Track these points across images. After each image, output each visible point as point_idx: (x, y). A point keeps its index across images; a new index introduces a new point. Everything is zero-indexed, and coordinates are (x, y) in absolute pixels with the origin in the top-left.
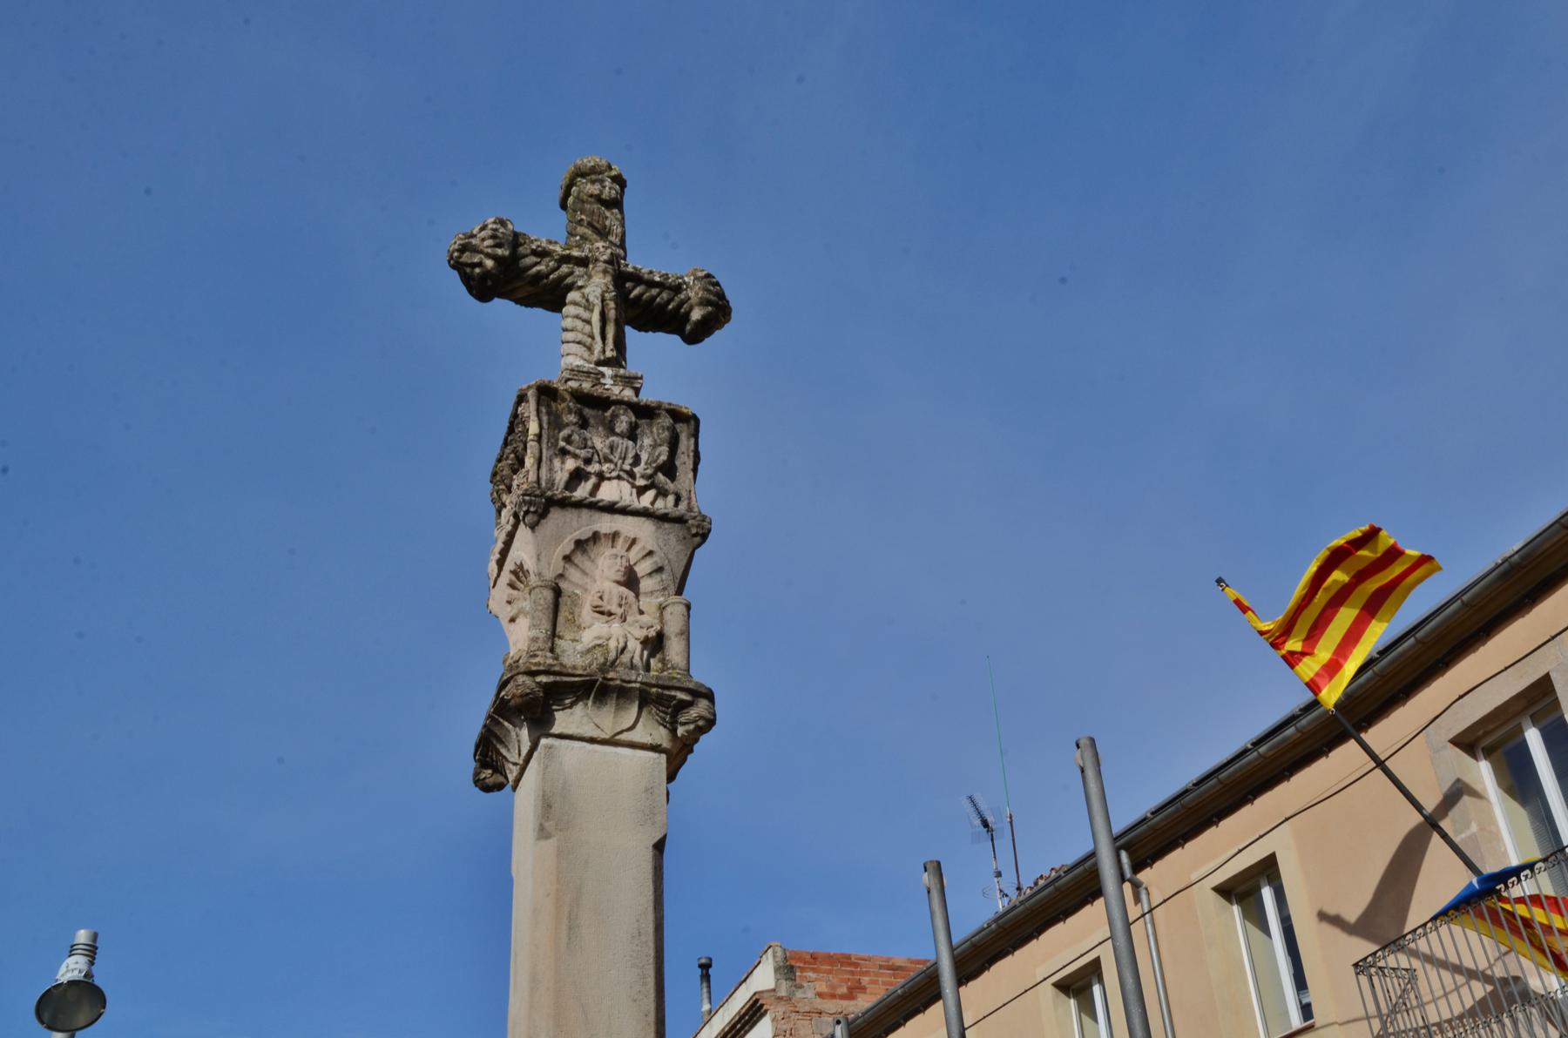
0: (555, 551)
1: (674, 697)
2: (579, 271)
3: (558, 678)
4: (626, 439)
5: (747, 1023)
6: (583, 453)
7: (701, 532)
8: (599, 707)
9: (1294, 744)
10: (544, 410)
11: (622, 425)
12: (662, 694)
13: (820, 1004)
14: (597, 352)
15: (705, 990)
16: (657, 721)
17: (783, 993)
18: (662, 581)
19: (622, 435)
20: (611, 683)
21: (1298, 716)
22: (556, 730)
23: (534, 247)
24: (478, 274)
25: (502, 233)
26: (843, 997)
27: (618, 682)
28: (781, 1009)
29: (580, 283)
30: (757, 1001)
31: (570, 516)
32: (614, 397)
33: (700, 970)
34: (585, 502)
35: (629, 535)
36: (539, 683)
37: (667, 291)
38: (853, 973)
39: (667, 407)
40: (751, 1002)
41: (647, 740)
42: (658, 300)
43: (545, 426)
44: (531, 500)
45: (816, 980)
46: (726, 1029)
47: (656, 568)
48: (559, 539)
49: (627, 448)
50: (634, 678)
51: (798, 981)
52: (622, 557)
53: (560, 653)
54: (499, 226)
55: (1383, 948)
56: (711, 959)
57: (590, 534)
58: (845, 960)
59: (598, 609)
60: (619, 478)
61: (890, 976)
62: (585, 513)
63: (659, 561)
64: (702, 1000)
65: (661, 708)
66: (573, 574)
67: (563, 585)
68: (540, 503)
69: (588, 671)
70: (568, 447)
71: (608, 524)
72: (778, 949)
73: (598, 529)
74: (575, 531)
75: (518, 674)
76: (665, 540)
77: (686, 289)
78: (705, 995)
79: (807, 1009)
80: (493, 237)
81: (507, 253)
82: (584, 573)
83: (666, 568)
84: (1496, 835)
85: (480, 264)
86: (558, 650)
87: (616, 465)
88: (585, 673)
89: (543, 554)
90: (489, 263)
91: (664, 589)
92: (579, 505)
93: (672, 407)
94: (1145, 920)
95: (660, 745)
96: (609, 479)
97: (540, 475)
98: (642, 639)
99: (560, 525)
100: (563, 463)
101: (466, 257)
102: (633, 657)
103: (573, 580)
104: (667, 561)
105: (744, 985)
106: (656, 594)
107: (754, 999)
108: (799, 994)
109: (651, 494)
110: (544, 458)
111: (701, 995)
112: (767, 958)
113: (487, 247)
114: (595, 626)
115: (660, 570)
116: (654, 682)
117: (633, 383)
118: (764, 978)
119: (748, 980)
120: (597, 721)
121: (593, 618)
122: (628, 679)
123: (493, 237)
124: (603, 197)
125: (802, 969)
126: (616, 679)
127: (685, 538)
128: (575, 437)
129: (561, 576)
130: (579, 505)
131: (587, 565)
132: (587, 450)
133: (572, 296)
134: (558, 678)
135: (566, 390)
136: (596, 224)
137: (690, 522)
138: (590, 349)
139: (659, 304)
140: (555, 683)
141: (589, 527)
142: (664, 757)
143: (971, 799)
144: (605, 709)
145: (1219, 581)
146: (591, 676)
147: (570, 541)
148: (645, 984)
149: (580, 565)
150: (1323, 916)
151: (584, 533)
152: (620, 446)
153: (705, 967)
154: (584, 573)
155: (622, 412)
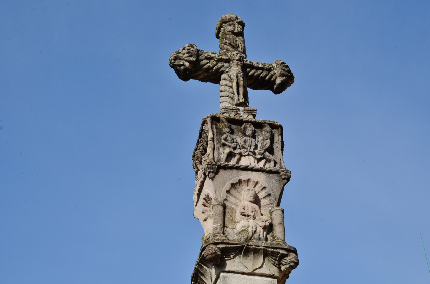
1: (279, 253)
2: (226, 65)
3: (227, 246)
6: (233, 145)
10: (214, 127)
11: (249, 132)
16: (272, 264)
18: (270, 200)
19: (249, 136)
20: (251, 247)
22: (227, 269)
23: (206, 56)
25: (192, 50)
27: (254, 246)
29: (227, 70)
31: (228, 172)
34: (234, 166)
36: (218, 248)
39: (268, 122)
41: (268, 272)
42: (261, 75)
43: (215, 134)
44: (211, 167)
48: (224, 184)
50: (260, 244)
52: (252, 190)
54: (190, 48)
59: (243, 214)
60: (249, 155)
62: (235, 171)
63: (268, 191)
65: (273, 258)
66: (231, 199)
67: (227, 204)
69: (240, 242)
70: (226, 143)
71: (245, 176)
74: (231, 180)
77: (273, 70)
80: (188, 52)
81: (194, 59)
82: (236, 198)
86: (226, 233)
87: (247, 149)
88: (239, 243)
90: (187, 64)
91: (272, 204)
92: (232, 168)
93: (270, 122)
95: (274, 275)
96: (244, 156)
99: (224, 177)
103: (231, 201)
104: (272, 191)
106: (268, 206)
109: (263, 161)
113: (186, 57)
117: (252, 113)
120: (245, 264)
121: (241, 218)
124: (235, 31)
127: (279, 181)
128: (229, 138)
129: (226, 200)
130: (232, 168)
131: (237, 194)
133: (224, 76)
134: (227, 246)
135: (224, 118)
136: (232, 44)
139: (262, 77)
141: (237, 178)
147: (229, 184)
149: (234, 194)
151: (235, 180)
154: (236, 198)
155: (248, 126)
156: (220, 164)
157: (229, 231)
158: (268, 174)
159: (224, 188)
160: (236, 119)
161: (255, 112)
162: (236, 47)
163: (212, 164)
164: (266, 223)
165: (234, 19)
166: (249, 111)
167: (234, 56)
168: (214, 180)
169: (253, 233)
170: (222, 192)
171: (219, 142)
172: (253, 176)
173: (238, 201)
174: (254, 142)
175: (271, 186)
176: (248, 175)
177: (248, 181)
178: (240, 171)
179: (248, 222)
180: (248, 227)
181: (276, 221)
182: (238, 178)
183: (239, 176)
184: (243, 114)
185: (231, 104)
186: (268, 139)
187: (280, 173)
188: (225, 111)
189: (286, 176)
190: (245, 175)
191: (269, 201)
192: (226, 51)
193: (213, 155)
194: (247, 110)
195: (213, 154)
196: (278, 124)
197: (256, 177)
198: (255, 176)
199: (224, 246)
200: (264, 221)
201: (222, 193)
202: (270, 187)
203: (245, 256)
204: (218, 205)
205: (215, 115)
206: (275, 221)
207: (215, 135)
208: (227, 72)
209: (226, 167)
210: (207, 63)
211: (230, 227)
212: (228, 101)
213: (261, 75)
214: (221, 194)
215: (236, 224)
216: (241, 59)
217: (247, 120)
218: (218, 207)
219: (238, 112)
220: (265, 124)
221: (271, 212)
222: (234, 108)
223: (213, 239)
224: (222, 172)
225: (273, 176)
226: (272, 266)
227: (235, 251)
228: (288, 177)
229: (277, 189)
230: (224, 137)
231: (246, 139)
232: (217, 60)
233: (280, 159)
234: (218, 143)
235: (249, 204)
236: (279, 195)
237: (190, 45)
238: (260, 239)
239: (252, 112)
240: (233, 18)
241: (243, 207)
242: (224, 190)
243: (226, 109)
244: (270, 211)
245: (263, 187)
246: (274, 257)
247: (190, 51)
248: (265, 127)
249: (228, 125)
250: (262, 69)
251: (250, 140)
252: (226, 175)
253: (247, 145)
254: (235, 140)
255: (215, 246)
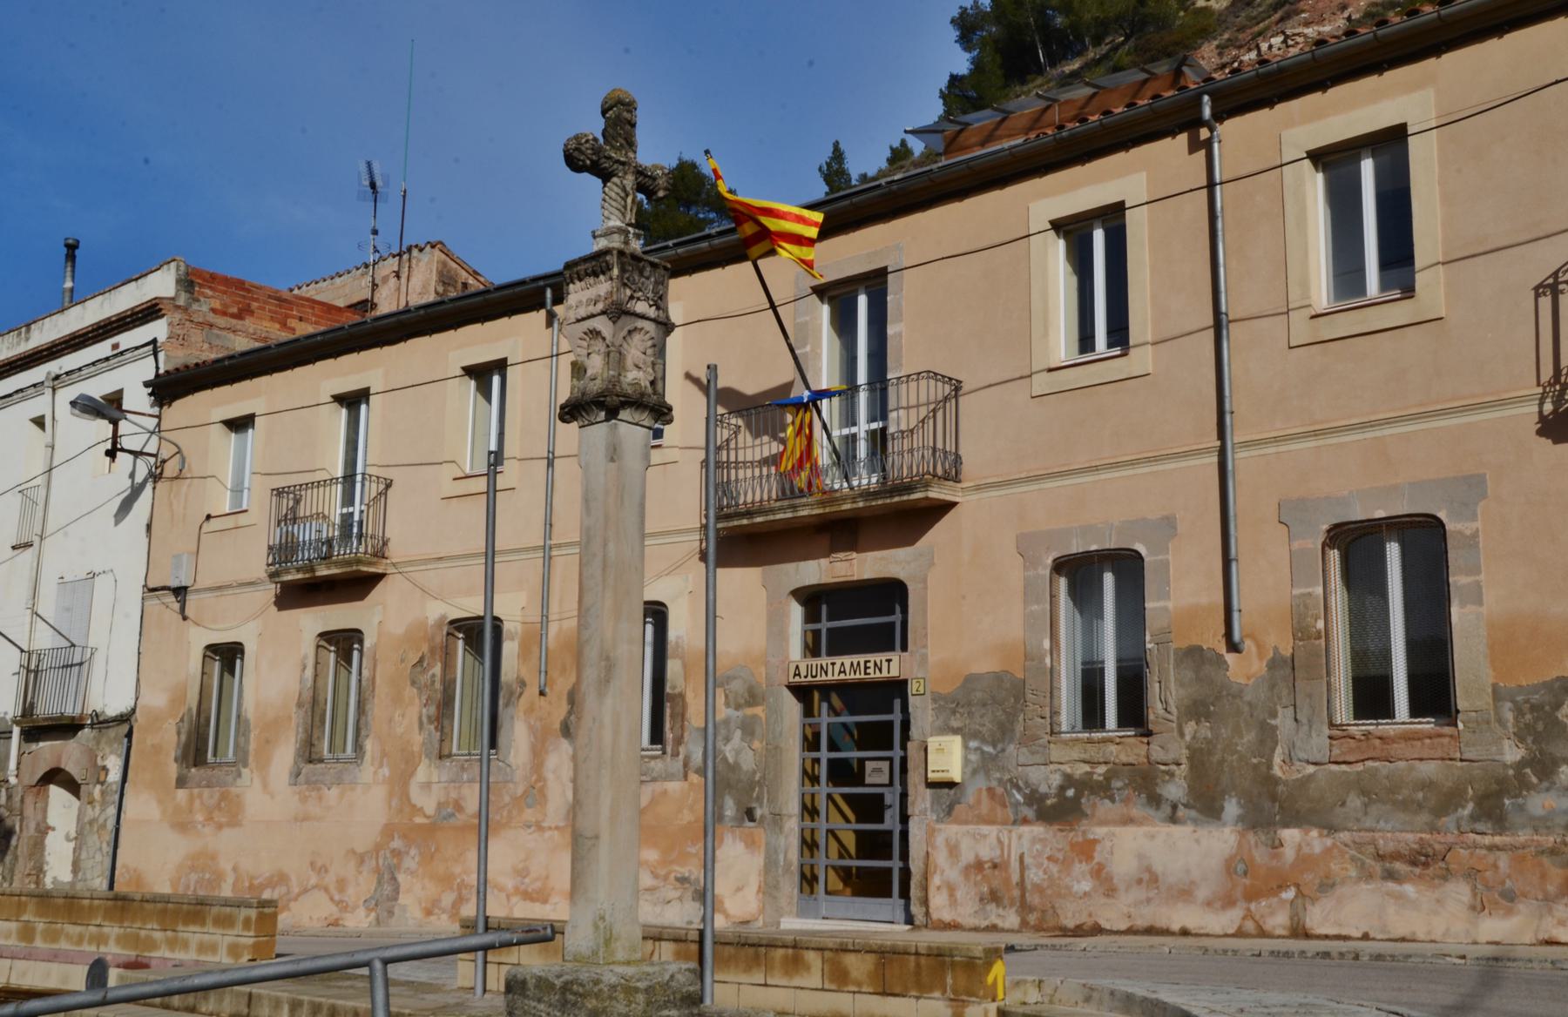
2: (621, 167)
5: (138, 319)
9: (703, 253)
13: (212, 318)
14: (628, 218)
15: (69, 269)
17: (181, 302)
21: (714, 236)
22: (619, 417)
26: (233, 316)
28: (178, 316)
30: (157, 304)
33: (65, 249)
38: (244, 297)
40: (149, 304)
45: (212, 297)
46: (114, 319)
48: (622, 329)
51: (196, 295)
55: (730, 413)
56: (78, 242)
58: (240, 285)
61: (276, 306)
64: (65, 277)
72: (182, 264)
78: (69, 274)
79: (201, 320)
84: (819, 356)
85: (583, 161)
90: (588, 162)
94: (558, 349)
101: (576, 154)
105: (134, 283)
107: (154, 302)
108: (195, 307)
111: (65, 272)
112: (169, 269)
118: (162, 284)
119: (140, 281)
123: (592, 149)
125: (201, 286)
133: (615, 179)
138: (624, 217)
143: (369, 164)
145: (707, 152)
150: (688, 376)
151: (630, 327)
153: (72, 248)
177: (642, 329)
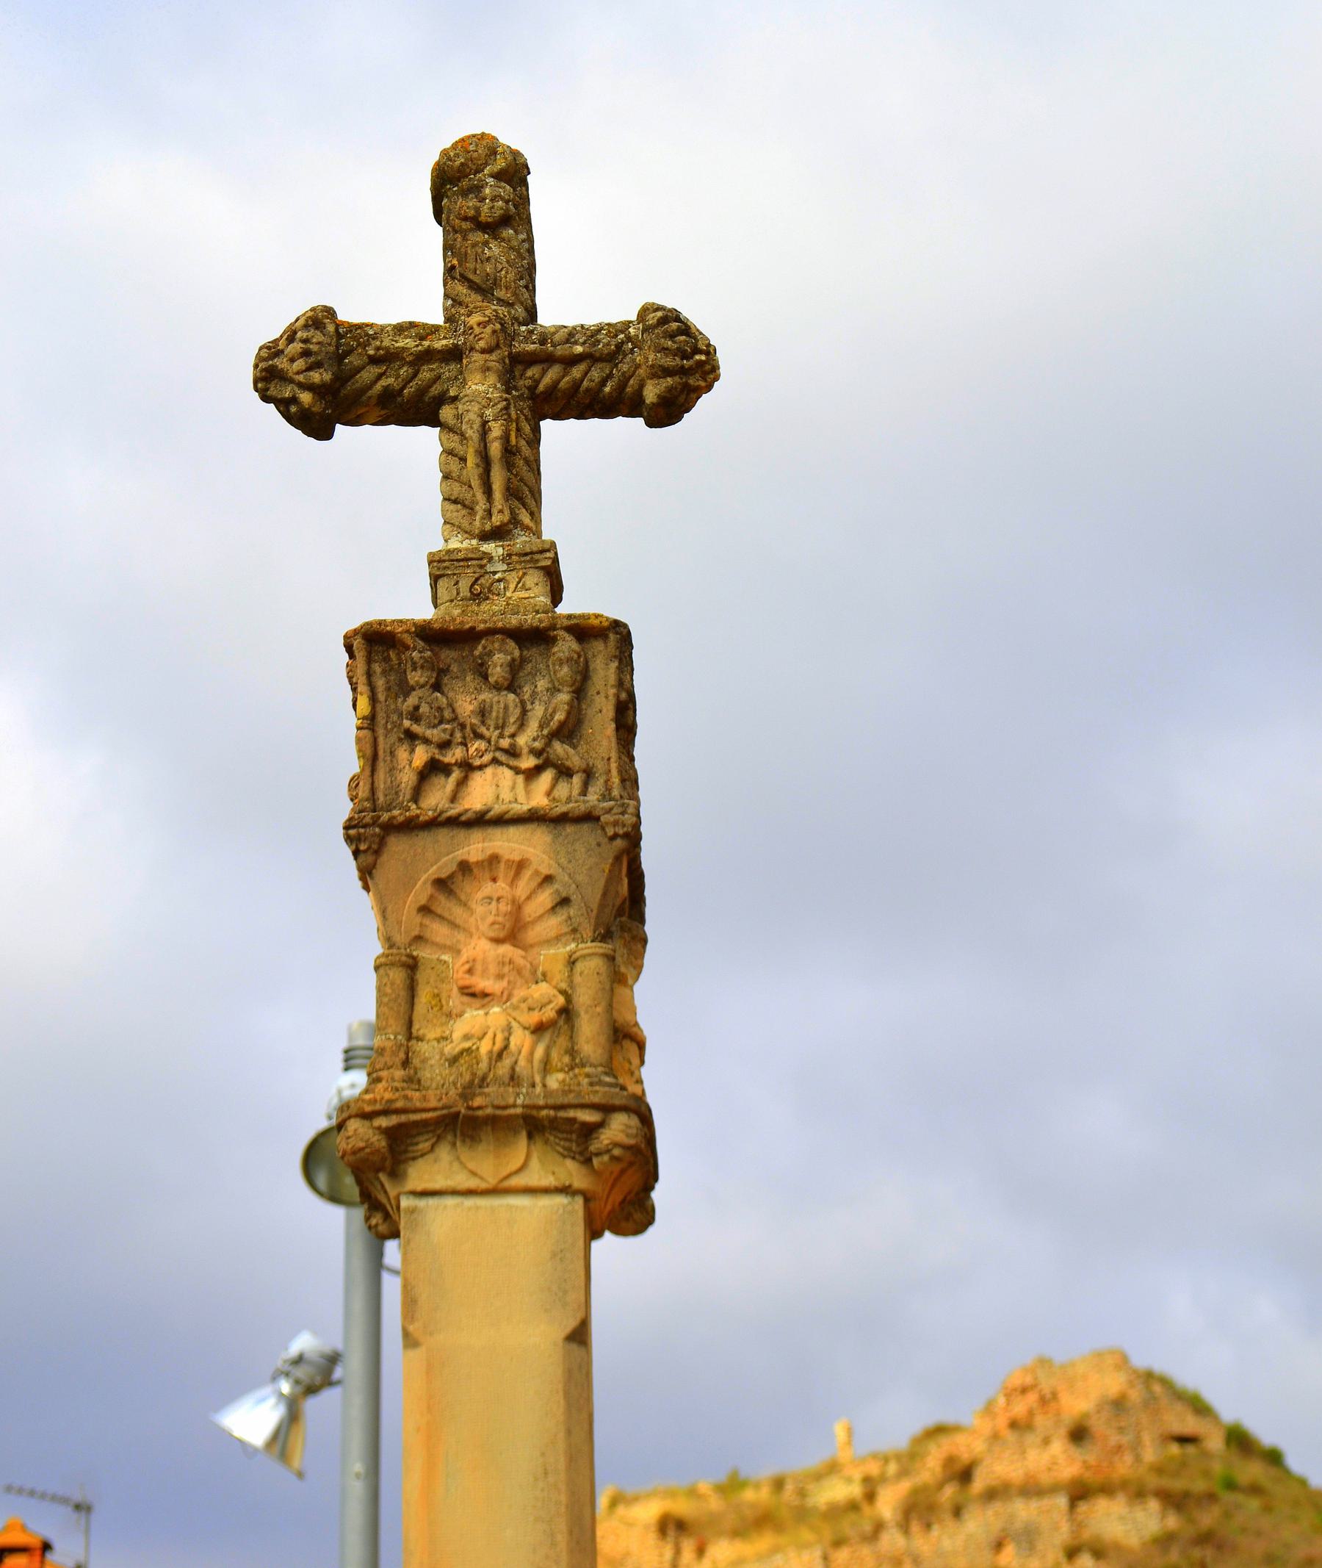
0: (405, 903)
1: (573, 1120)
2: (449, 370)
3: (403, 1118)
4: (505, 692)
6: (436, 734)
7: (621, 832)
8: (470, 1147)
10: (377, 668)
11: (498, 666)
12: (556, 1118)
16: (559, 1152)
18: (570, 918)
19: (497, 688)
20: (480, 1113)
23: (371, 352)
24: (295, 413)
25: (319, 343)
27: (489, 1111)
29: (452, 393)
31: (423, 841)
32: (482, 626)
34: (440, 819)
35: (512, 857)
36: (379, 1128)
37: (600, 365)
39: (566, 623)
41: (549, 1181)
42: (585, 383)
43: (381, 697)
44: (359, 834)
47: (558, 900)
48: (408, 884)
49: (506, 708)
50: (511, 1101)
52: (498, 899)
53: (418, 1065)
54: (312, 332)
57: (454, 867)
59: (466, 991)
60: (495, 761)
62: (443, 835)
63: (561, 889)
65: (561, 1135)
66: (438, 931)
67: (423, 953)
68: (374, 835)
69: (444, 1100)
70: (416, 728)
71: (480, 845)
73: (465, 857)
74: (432, 866)
75: (349, 1117)
76: (568, 853)
77: (632, 351)
80: (306, 353)
81: (327, 377)
82: (454, 925)
83: (573, 898)
86: (416, 1062)
87: (489, 742)
88: (440, 1104)
89: (389, 909)
91: (574, 931)
92: (435, 823)
93: (575, 621)
95: (570, 1186)
96: (481, 768)
97: (376, 784)
98: (532, 1028)
99: (409, 860)
100: (412, 751)
102: (516, 1062)
103: (437, 939)
104: (574, 886)
106: (564, 940)
109: (547, 777)
110: (381, 753)
113: (298, 373)
114: (466, 1015)
115: (564, 902)
116: (541, 1102)
117: (537, 561)
120: (471, 1165)
121: (463, 1003)
122: (503, 1103)
124: (482, 219)
126: (486, 1106)
127: (599, 845)
128: (424, 709)
129: (419, 938)
130: (435, 823)
131: (457, 913)
132: (444, 726)
134: (403, 1118)
135: (408, 631)
136: (471, 276)
137: (602, 819)
139: (588, 390)
140: (401, 1126)
141: (451, 856)
142: (579, 1201)
144: (480, 1148)
146: (450, 1107)
147: (425, 883)
148: (553, 1544)
149: (446, 915)
151: (444, 866)
152: (495, 707)
154: (454, 925)
155: (497, 645)
156: (389, 819)
157: (425, 1053)
158: (560, 828)
159: (410, 898)
160: (451, 630)
161: (548, 555)
162: (484, 286)
163: (361, 824)
164: (541, 1013)
165: (480, 162)
166: (526, 554)
167: (473, 335)
168: (374, 875)
169: (494, 1057)
170: (405, 912)
171: (395, 726)
172: (506, 844)
173: (461, 936)
174: (514, 709)
175: (571, 867)
176: (490, 840)
178: (463, 830)
179: (486, 1014)
180: (480, 1035)
181: (581, 996)
182: (453, 858)
183: (458, 850)
184: (505, 571)
185: (466, 532)
186: (566, 689)
187: (598, 819)
188: (439, 569)
189: (620, 827)
190: (478, 843)
191: (566, 921)
192: (453, 306)
193: (373, 783)
194: (516, 555)
195: (370, 779)
196: (601, 622)
197: (516, 846)
198: (514, 839)
199: (391, 1121)
200: (535, 1006)
201: (404, 918)
202: (568, 871)
203: (467, 1140)
204: (387, 965)
205: (375, 626)
206: (579, 996)
207: (380, 702)
208: (455, 399)
209: (413, 823)
210: (379, 377)
211: (431, 1034)
212: (457, 523)
213: (585, 382)
214: (401, 922)
215: (452, 1022)
216: (505, 334)
217: (488, 625)
218: (388, 972)
219: (485, 565)
220: (554, 630)
221: (572, 962)
222: (470, 556)
223: (360, 1102)
224: (398, 847)
225: (576, 833)
226: (561, 1159)
227: (432, 1128)
228: (625, 829)
229: (591, 876)
230: (408, 707)
231: (485, 701)
232: (414, 360)
233: (607, 757)
234: (392, 729)
235: (490, 949)
236: (599, 896)
237: (310, 323)
238: (516, 1077)
239: (537, 557)
240: (475, 159)
241: (467, 967)
242: (409, 907)
243: (444, 561)
244: (570, 957)
245: (543, 876)
246: (563, 1132)
247: (309, 348)
248: (557, 640)
249: (421, 657)
250: (590, 358)
251: (499, 702)
252: (415, 850)
253: (491, 723)
254: (447, 714)
255: (367, 1123)
